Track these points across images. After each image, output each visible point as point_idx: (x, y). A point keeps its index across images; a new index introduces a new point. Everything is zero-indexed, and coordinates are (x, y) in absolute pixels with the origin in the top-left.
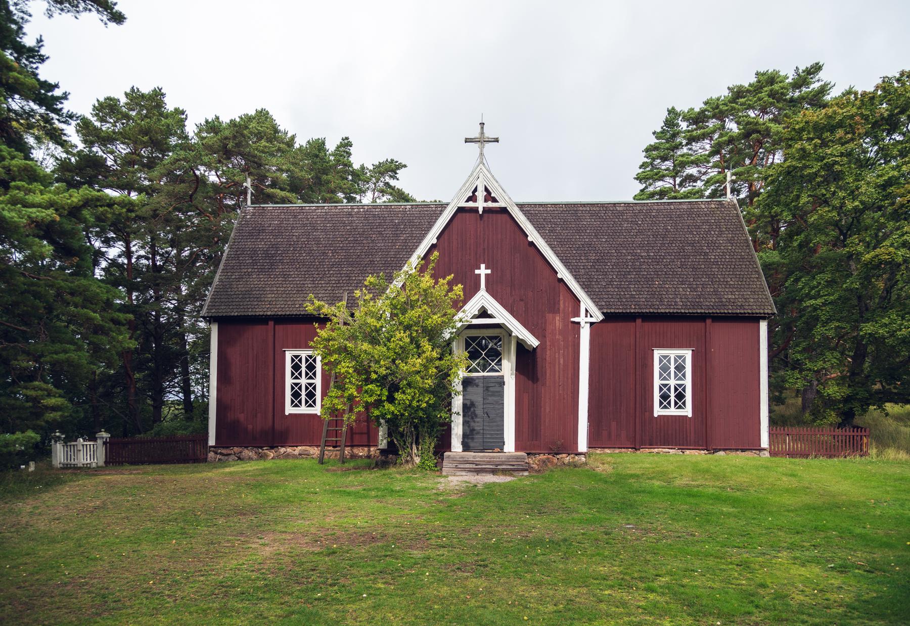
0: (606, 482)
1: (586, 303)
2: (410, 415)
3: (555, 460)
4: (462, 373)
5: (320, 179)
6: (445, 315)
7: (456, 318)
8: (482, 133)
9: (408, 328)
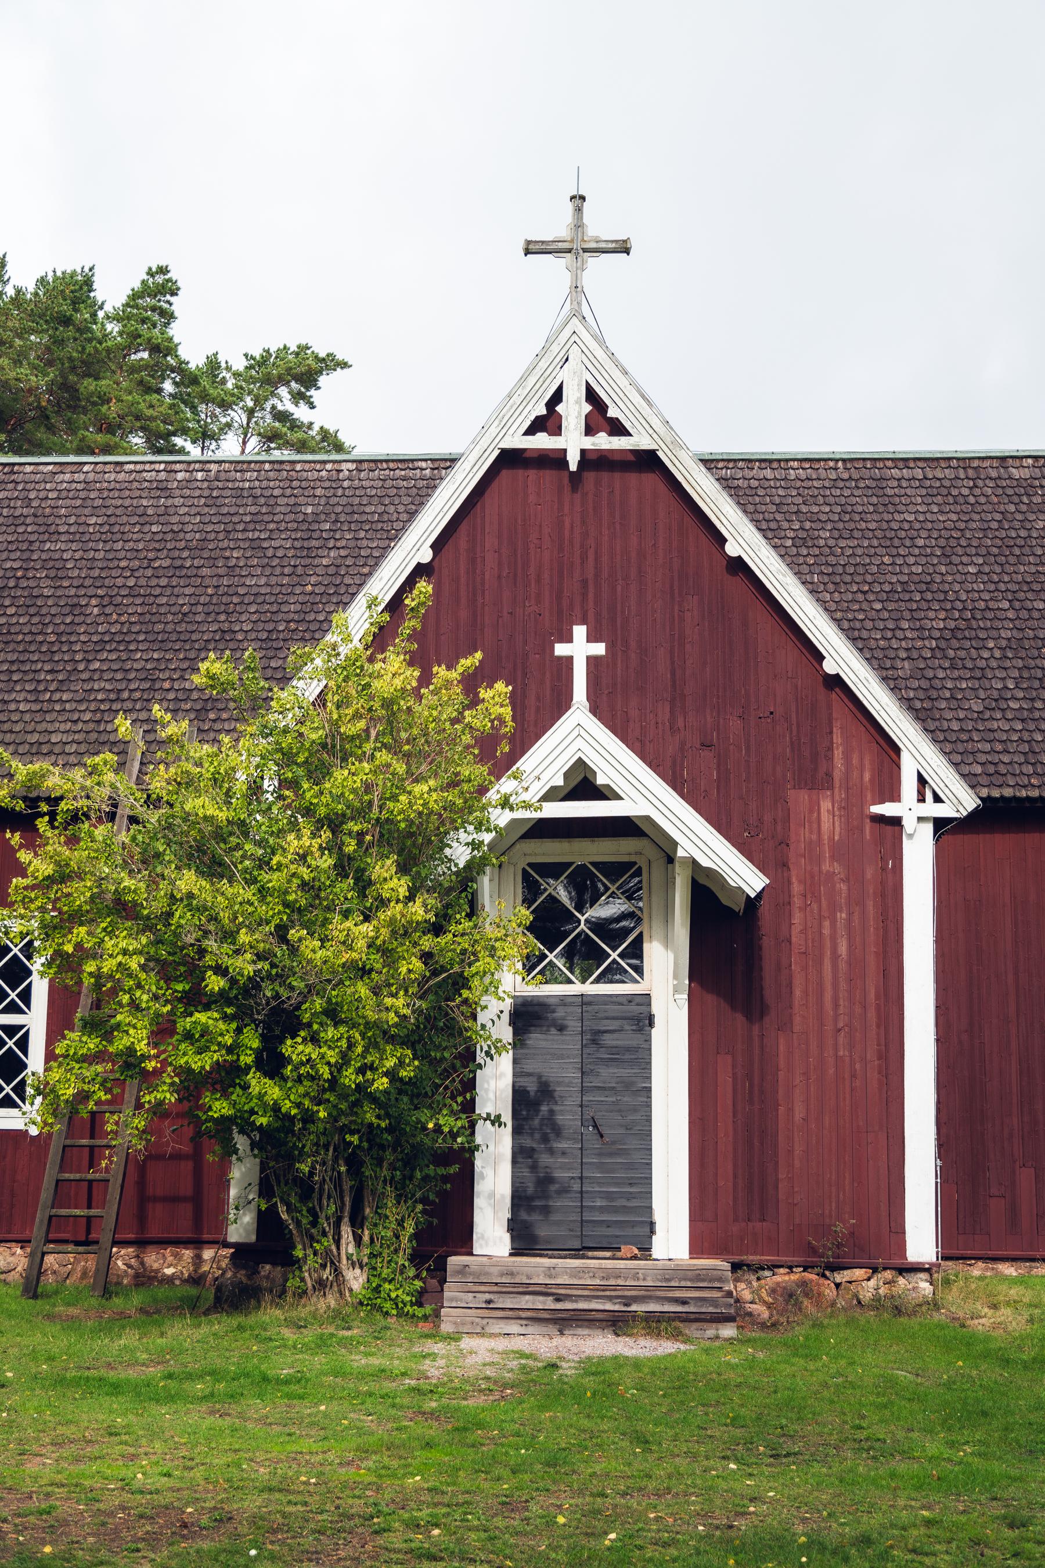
0: (1006, 1362)
1: (918, 753)
2: (333, 1118)
3: (830, 1292)
4: (512, 983)
5: (72, 390)
6: (453, 784)
7: (493, 795)
8: (579, 225)
9: (334, 823)
